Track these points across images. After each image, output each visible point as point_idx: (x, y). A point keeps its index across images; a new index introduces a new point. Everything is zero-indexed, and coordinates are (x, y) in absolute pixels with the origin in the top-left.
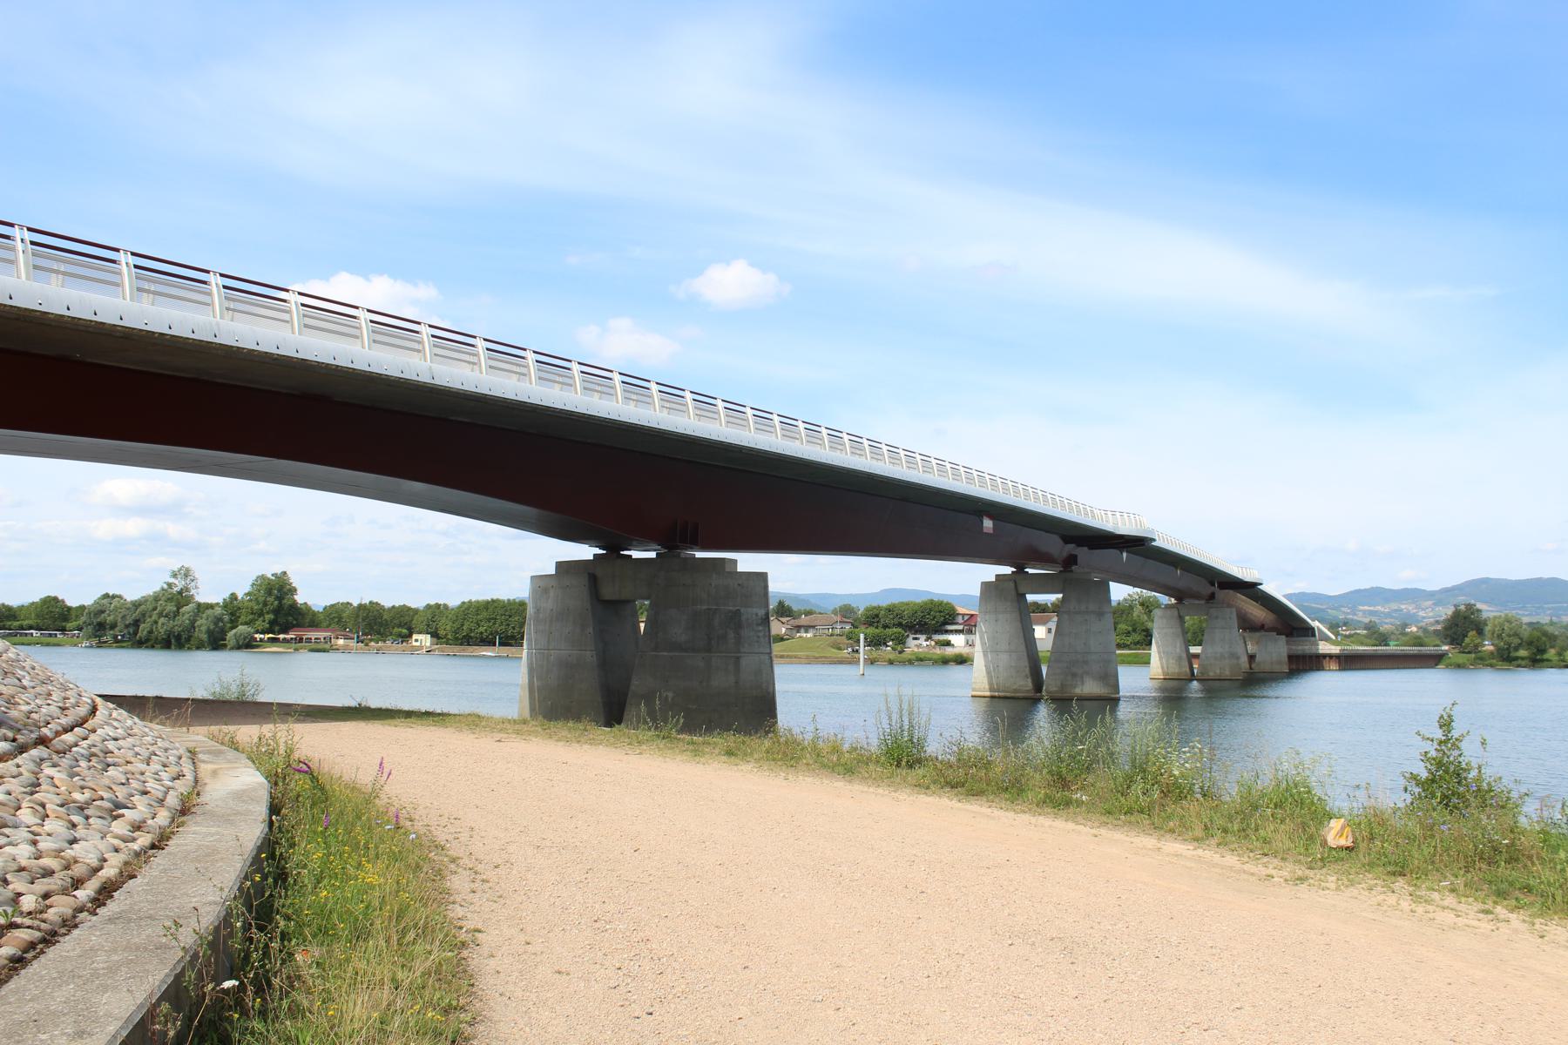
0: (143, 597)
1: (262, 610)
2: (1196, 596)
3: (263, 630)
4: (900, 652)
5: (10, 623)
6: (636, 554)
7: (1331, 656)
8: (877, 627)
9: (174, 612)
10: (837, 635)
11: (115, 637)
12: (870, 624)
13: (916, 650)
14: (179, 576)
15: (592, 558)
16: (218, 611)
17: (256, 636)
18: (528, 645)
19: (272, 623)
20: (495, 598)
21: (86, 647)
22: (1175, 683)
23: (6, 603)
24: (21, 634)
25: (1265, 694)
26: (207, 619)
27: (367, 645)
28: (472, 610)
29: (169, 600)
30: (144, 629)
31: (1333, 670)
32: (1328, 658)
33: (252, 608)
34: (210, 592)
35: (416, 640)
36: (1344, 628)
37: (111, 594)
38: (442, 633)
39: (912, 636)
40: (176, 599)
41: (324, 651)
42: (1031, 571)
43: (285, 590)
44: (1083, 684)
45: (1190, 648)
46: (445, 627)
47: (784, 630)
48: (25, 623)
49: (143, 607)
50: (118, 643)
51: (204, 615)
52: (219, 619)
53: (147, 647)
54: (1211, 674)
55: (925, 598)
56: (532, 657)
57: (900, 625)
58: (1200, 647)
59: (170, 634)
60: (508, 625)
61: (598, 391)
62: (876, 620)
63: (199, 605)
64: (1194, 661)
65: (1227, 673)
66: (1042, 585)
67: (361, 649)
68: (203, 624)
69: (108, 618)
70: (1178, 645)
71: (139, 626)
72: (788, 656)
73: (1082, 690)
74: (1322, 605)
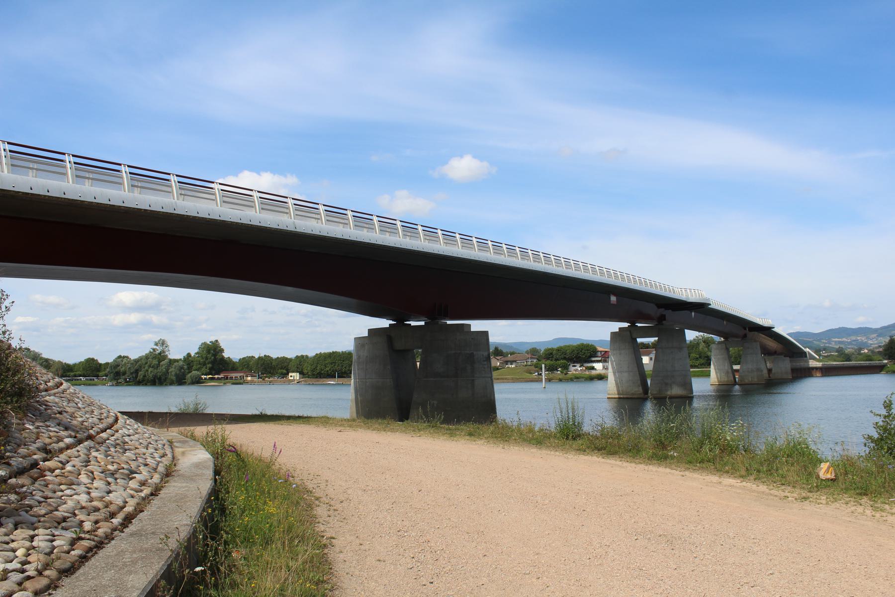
0: (139, 357)
4: (566, 374)
6: (413, 323)
7: (817, 368)
8: (552, 360)
9: (157, 364)
11: (125, 379)
14: (159, 345)
15: (388, 326)
16: (181, 363)
17: (202, 376)
19: (211, 369)
20: (334, 351)
24: (75, 380)
27: (264, 380)
28: (322, 358)
29: (154, 358)
31: (818, 376)
32: (815, 370)
33: (199, 361)
34: (176, 353)
35: (291, 376)
36: (824, 352)
37: (122, 356)
38: (305, 371)
39: (572, 365)
40: (157, 357)
44: (671, 389)
46: (307, 368)
47: (498, 363)
49: (140, 362)
50: (128, 383)
52: (182, 368)
54: (746, 381)
55: (579, 343)
56: (356, 384)
57: (565, 358)
58: (739, 366)
59: (155, 377)
60: (342, 366)
62: (551, 356)
63: (170, 360)
64: (735, 373)
65: (756, 380)
66: (646, 333)
67: (261, 382)
68: (173, 370)
70: (726, 364)
71: (138, 373)
72: (502, 379)
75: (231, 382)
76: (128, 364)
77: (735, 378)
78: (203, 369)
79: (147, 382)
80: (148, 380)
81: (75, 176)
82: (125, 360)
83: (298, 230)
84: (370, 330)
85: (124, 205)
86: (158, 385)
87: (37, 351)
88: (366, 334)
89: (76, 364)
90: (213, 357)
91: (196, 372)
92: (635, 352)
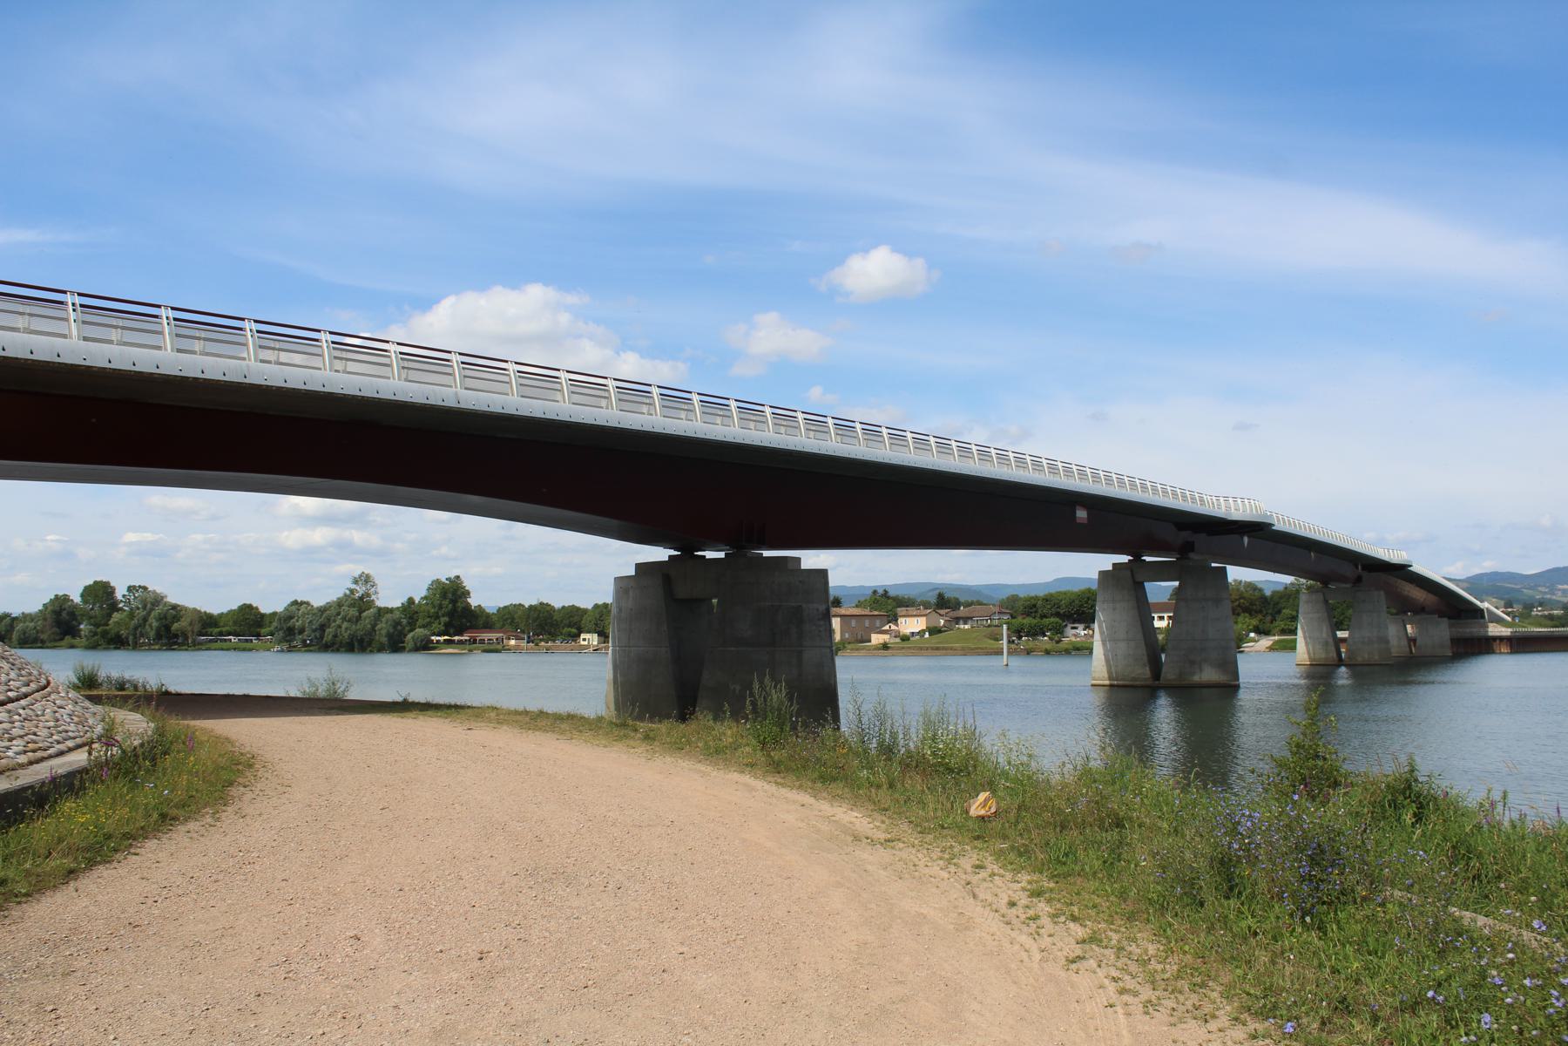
0: (327, 603)
1: (437, 613)
2: (1342, 579)
3: (439, 632)
4: (1058, 642)
5: (211, 630)
6: (710, 555)
7: (1501, 639)
8: (1034, 618)
9: (357, 617)
10: (996, 626)
11: (304, 641)
12: (1028, 614)
13: (1073, 639)
14: (360, 582)
15: (1111, 568)
16: (397, 615)
17: (433, 638)
18: (613, 643)
19: (447, 625)
21: (278, 651)
22: (1320, 669)
23: (208, 612)
24: (221, 640)
25: (1424, 679)
26: (387, 623)
27: (537, 645)
29: (352, 605)
30: (329, 632)
31: (1504, 653)
32: (1498, 641)
33: (429, 612)
34: (390, 596)
35: (584, 640)
36: (1539, 609)
37: (299, 601)
39: (1070, 626)
40: (358, 603)
41: (497, 651)
42: (1148, 559)
43: (459, 593)
44: (1201, 670)
45: (1338, 633)
47: (942, 622)
48: (224, 629)
49: (328, 612)
50: (307, 647)
51: (383, 620)
52: (397, 623)
53: (333, 651)
57: (1058, 615)
58: (1347, 632)
59: (352, 637)
61: (783, 425)
62: (1034, 609)
63: (380, 609)
64: (1341, 645)
65: (1377, 657)
66: (1160, 572)
67: (532, 648)
68: (383, 627)
69: (297, 624)
70: (1325, 629)
71: (324, 631)
72: (944, 648)
73: (1200, 678)
74: (1516, 584)
75: (482, 648)
76: (308, 614)
77: (1339, 653)
78: (434, 625)
79: (340, 646)
80: (341, 643)
81: (258, 348)
82: (303, 609)
83: (463, 406)
84: (638, 566)
85: (158, 371)
86: (359, 652)
87: (159, 590)
88: (632, 572)
89: (222, 613)
90: (450, 605)
91: (422, 630)
92: (1138, 607)
